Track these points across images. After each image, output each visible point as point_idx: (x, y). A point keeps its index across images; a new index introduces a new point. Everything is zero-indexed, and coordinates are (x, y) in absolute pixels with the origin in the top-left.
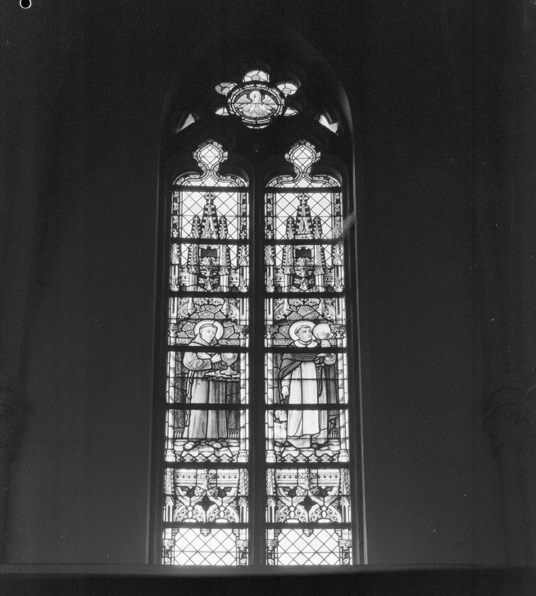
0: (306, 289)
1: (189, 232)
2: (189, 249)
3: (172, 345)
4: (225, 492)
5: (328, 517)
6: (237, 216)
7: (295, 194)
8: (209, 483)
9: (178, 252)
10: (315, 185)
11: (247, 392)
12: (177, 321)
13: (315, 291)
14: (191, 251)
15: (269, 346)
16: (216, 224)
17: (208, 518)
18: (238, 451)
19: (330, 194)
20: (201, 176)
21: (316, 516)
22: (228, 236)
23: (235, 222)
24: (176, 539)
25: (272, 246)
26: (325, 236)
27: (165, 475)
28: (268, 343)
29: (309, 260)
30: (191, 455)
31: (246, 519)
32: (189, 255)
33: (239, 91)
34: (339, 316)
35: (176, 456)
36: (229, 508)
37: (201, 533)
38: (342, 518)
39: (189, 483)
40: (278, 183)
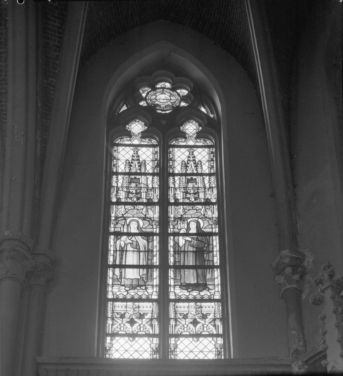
0: (194, 200)
1: (180, 170)
2: (180, 178)
3: (112, 232)
4: (144, 316)
5: (124, 330)
6: (152, 161)
7: (131, 147)
8: (196, 311)
9: (173, 181)
10: (197, 144)
11: (158, 258)
12: (174, 219)
13: (141, 201)
14: (124, 179)
15: (171, 232)
16: (195, 165)
17: (197, 330)
18: (214, 292)
19: (207, 149)
20: (131, 139)
21: (200, 330)
22: (146, 171)
23: (151, 164)
24: (178, 344)
25: (172, 177)
26: (148, 171)
27: (169, 307)
28: (170, 230)
29: (195, 184)
30: (185, 295)
31: (157, 332)
32: (180, 182)
33: (153, 92)
34: (214, 216)
35: (113, 295)
36: (146, 325)
37: (193, 340)
38: (153, 331)
39: (121, 311)
40: (121, 141)
